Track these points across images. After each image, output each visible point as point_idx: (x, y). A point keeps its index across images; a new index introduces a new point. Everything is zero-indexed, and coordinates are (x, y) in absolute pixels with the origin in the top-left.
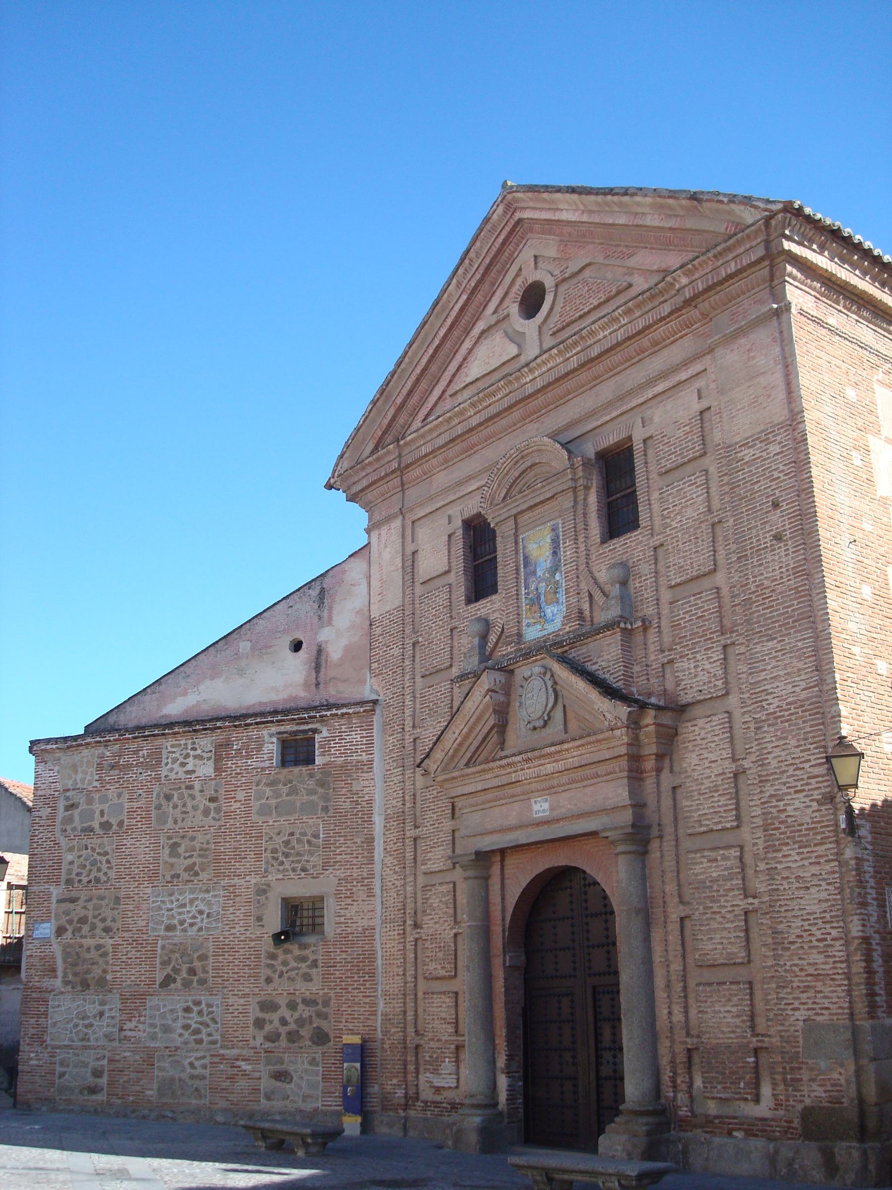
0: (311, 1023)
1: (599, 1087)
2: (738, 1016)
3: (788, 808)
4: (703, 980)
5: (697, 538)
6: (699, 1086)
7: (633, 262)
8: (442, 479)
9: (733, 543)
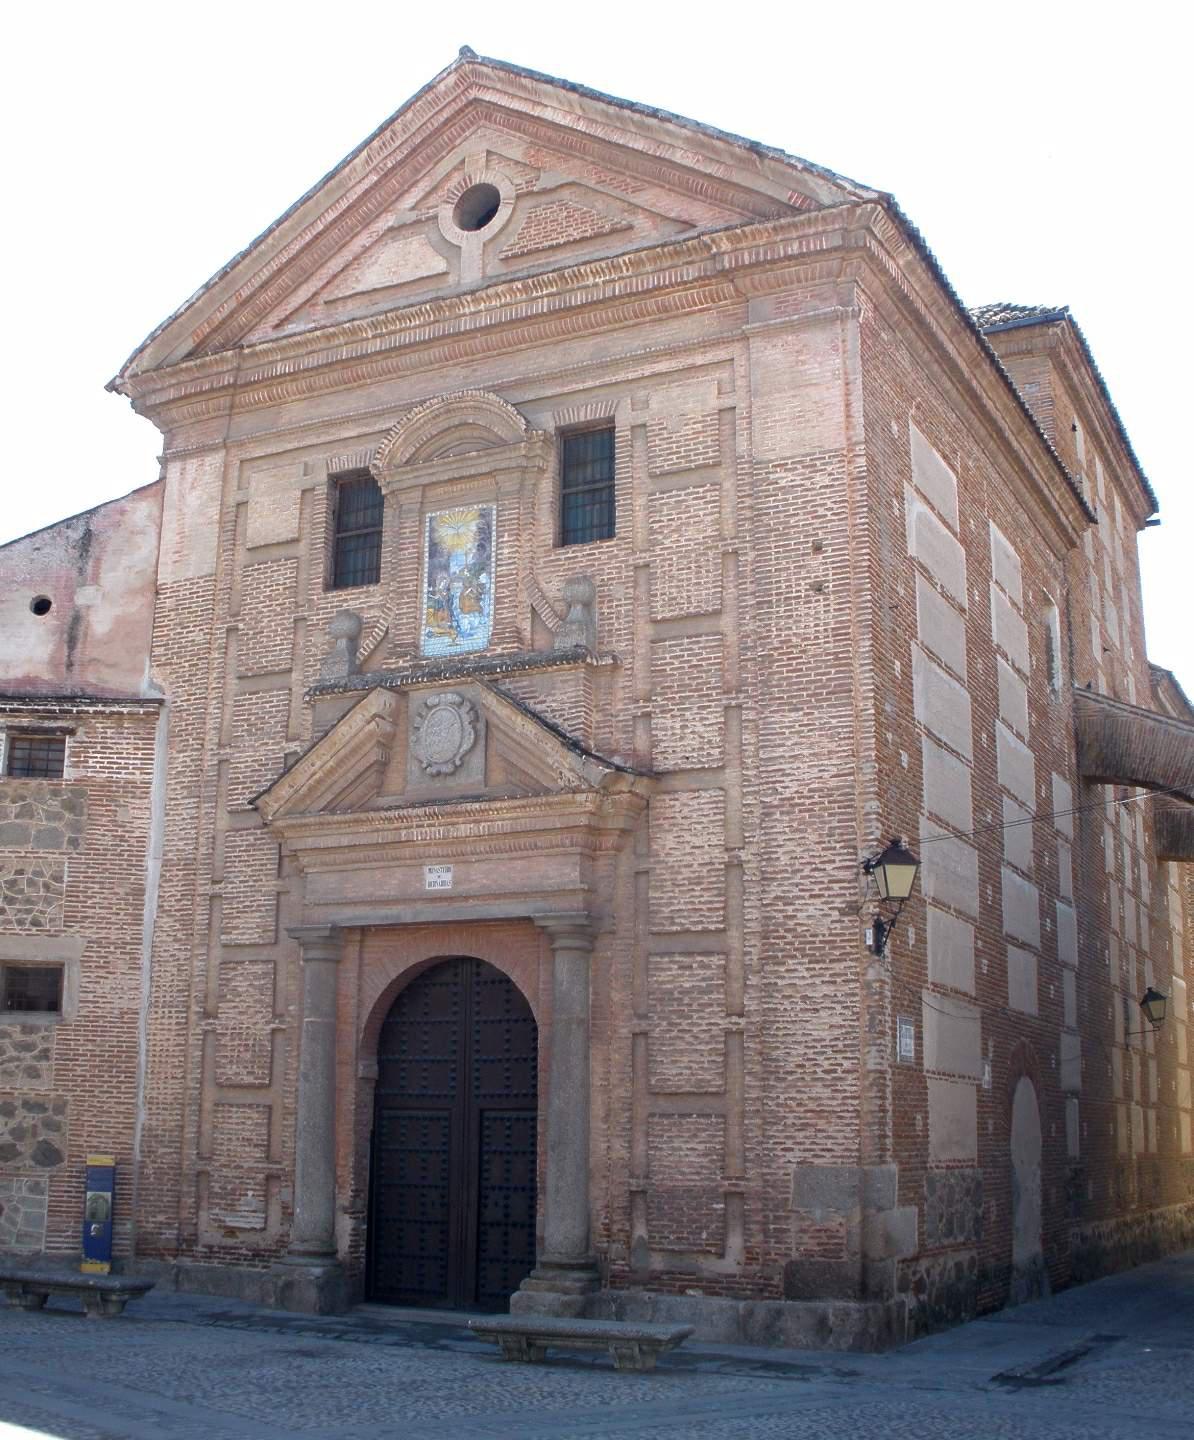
0: (35, 1135)
1: (480, 1235)
2: (705, 1155)
3: (799, 915)
4: (657, 1111)
5: (700, 567)
6: (641, 1237)
7: (640, 199)
8: (296, 412)
9: (752, 582)
